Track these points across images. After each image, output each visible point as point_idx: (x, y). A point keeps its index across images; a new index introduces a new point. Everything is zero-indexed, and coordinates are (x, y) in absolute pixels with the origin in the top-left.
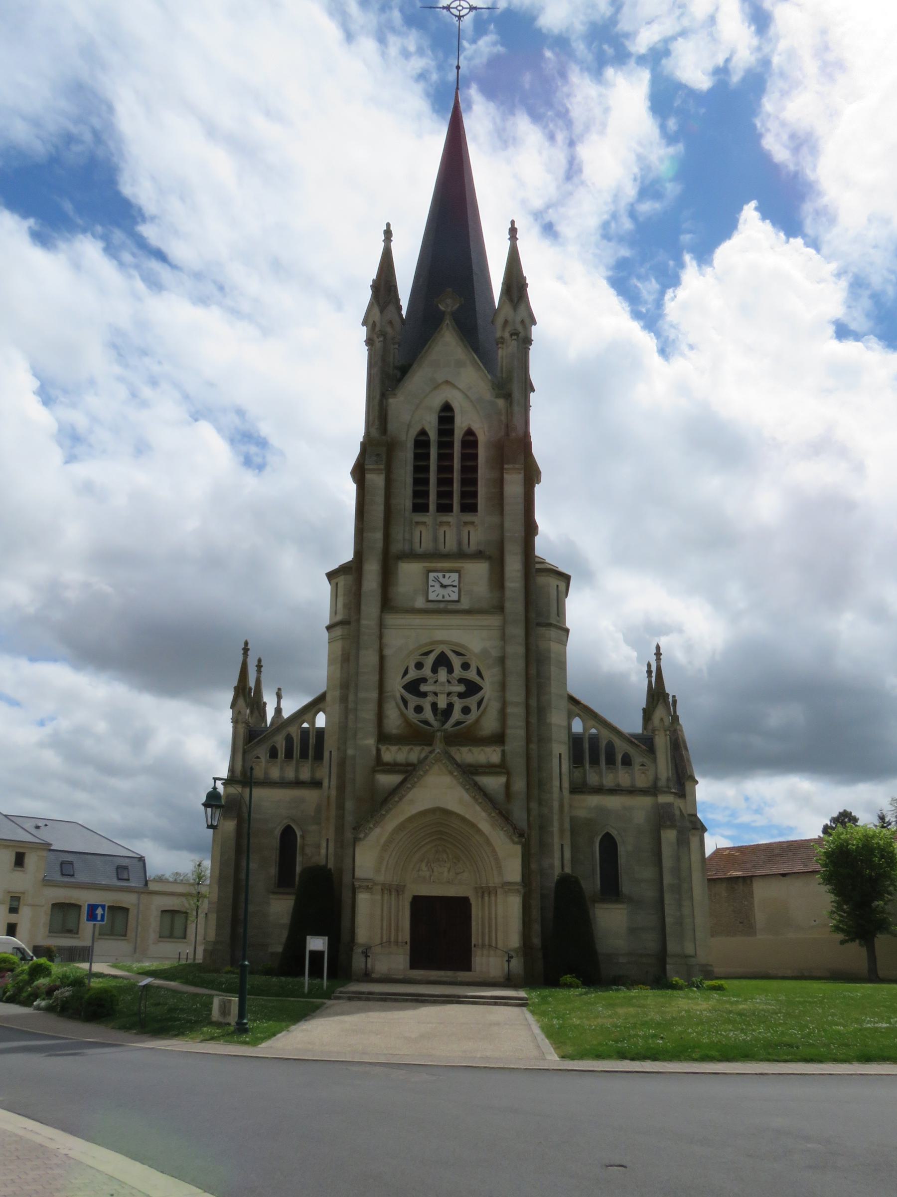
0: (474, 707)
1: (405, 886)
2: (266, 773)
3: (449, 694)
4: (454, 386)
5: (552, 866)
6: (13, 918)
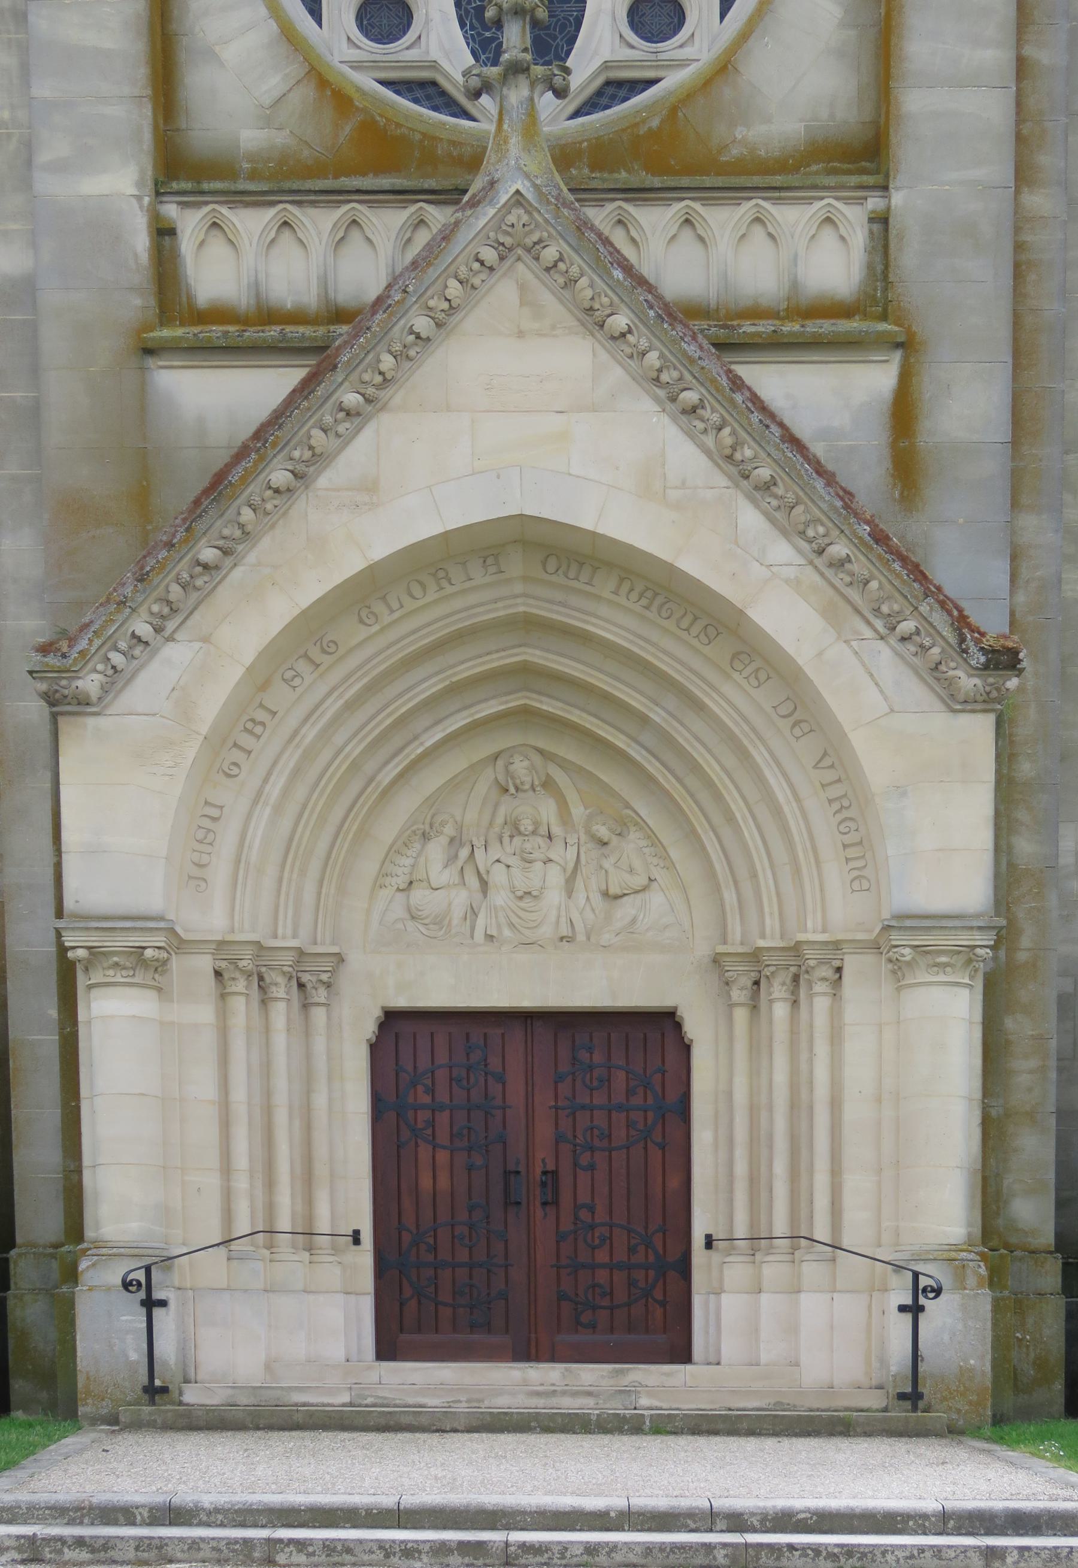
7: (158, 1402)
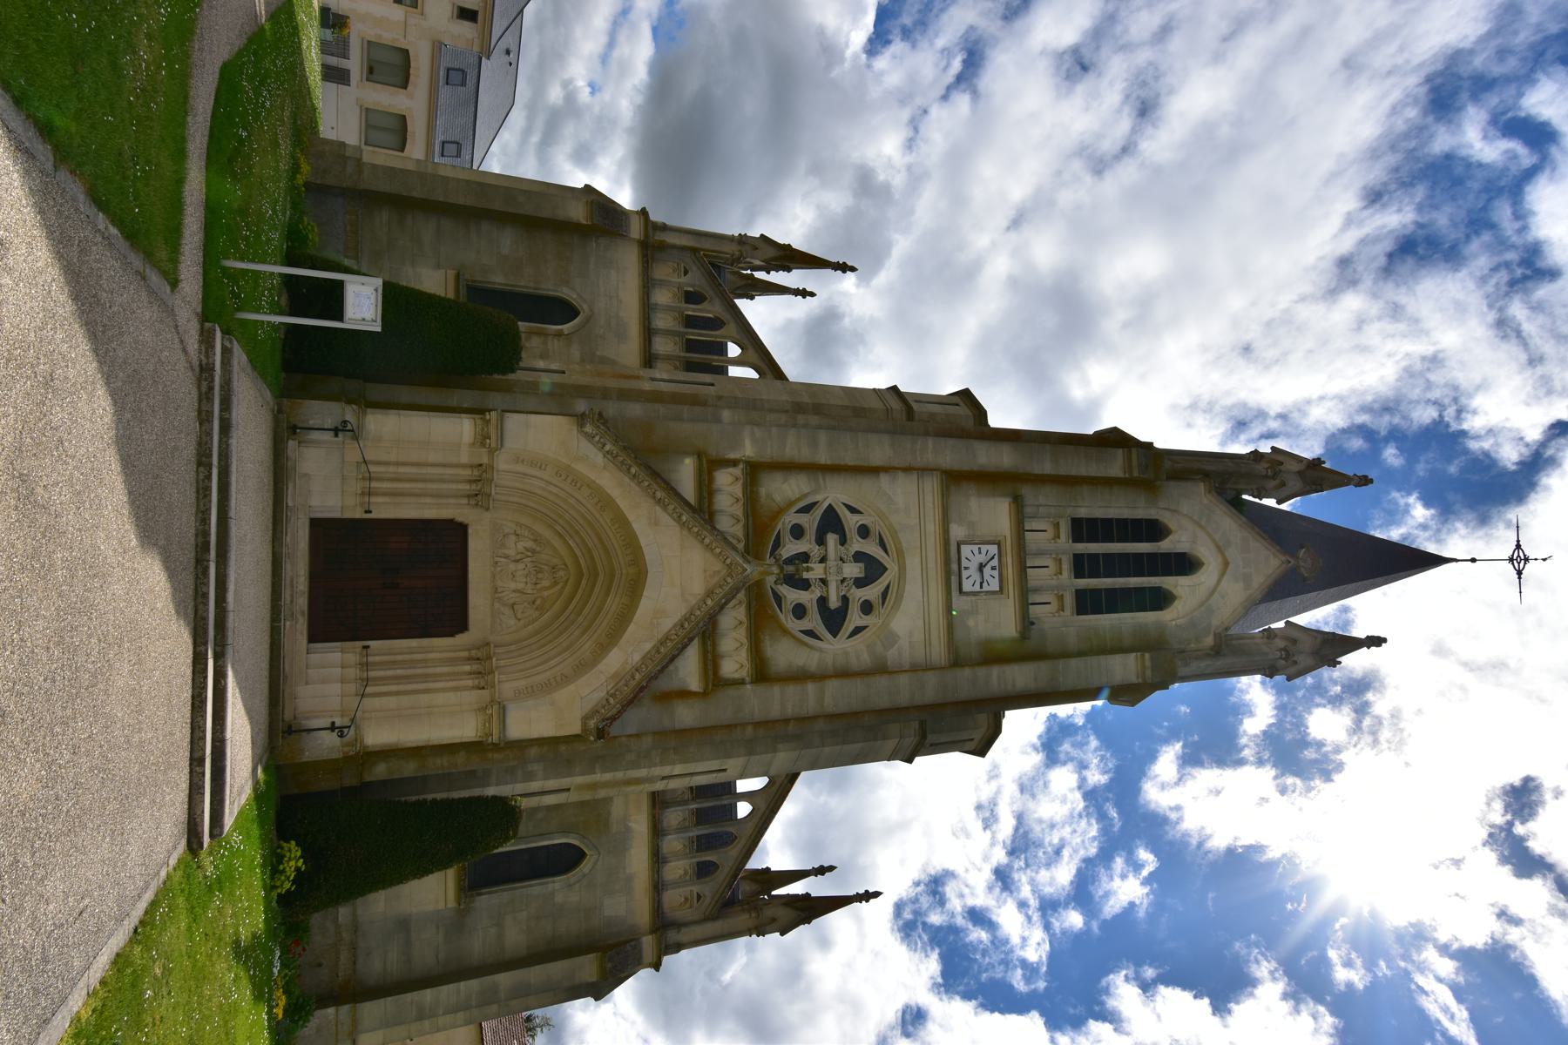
0: (805, 624)
1: (488, 509)
3: (824, 581)
5: (529, 777)
7: (285, 432)
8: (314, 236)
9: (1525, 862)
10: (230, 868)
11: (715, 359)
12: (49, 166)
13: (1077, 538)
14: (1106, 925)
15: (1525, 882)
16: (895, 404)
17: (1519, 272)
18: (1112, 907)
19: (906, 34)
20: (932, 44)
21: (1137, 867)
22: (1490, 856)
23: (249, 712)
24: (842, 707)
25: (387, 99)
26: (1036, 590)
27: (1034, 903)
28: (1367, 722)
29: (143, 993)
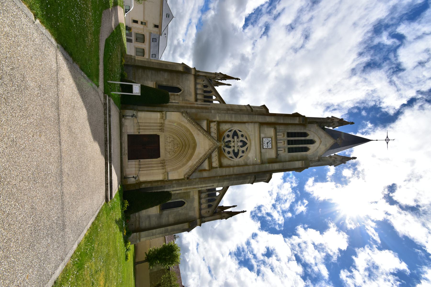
0: (230, 155)
2: (199, 83)
3: (234, 146)
4: (320, 144)
5: (173, 187)
6: (139, 22)
7: (122, 117)
8: (126, 76)
9: (392, 202)
10: (114, 205)
11: (210, 100)
12: (72, 62)
13: (288, 137)
14: (296, 216)
15: (392, 206)
16: (249, 108)
17: (395, 70)
18: (298, 212)
19: (252, 24)
20: (258, 25)
21: (304, 204)
22: (384, 201)
23: (117, 174)
24: (238, 173)
25: (140, 45)
26: (279, 148)
27: (281, 211)
28: (356, 172)
29: (98, 230)
